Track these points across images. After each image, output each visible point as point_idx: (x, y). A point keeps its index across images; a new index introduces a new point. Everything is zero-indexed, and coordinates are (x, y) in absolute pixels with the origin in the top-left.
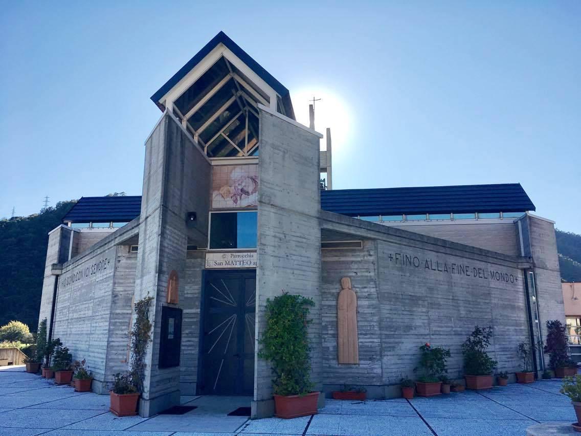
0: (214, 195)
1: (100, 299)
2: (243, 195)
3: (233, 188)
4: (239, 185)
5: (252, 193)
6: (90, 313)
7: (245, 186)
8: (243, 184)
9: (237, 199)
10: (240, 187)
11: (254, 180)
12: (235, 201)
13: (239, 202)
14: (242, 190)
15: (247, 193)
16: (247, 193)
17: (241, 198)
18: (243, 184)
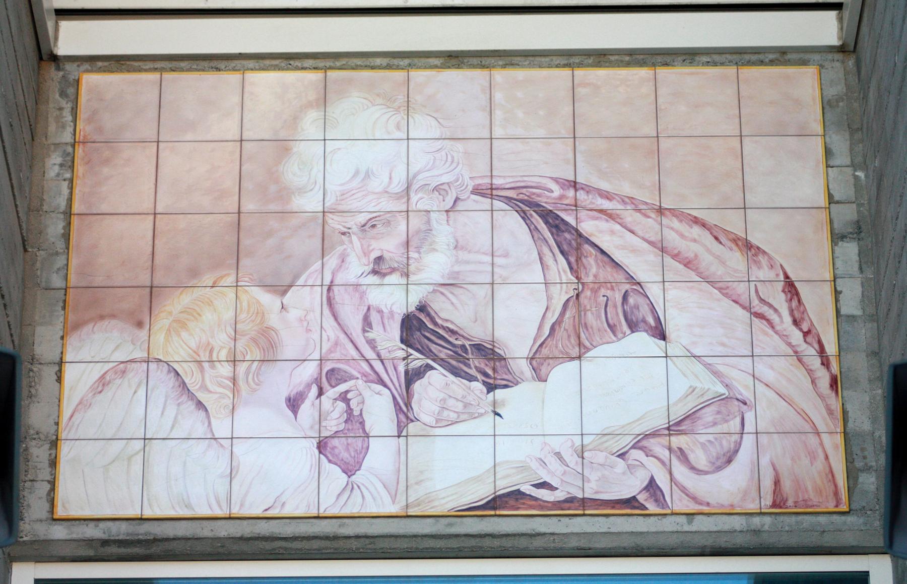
0: (78, 378)
2: (436, 386)
3: (305, 299)
4: (379, 267)
5: (540, 362)
7: (450, 285)
8: (434, 265)
9: (354, 420)
10: (394, 298)
11: (555, 226)
12: (341, 446)
13: (380, 456)
14: (416, 327)
15: (483, 363)
16: (483, 363)
17: (404, 412)
18: (434, 265)
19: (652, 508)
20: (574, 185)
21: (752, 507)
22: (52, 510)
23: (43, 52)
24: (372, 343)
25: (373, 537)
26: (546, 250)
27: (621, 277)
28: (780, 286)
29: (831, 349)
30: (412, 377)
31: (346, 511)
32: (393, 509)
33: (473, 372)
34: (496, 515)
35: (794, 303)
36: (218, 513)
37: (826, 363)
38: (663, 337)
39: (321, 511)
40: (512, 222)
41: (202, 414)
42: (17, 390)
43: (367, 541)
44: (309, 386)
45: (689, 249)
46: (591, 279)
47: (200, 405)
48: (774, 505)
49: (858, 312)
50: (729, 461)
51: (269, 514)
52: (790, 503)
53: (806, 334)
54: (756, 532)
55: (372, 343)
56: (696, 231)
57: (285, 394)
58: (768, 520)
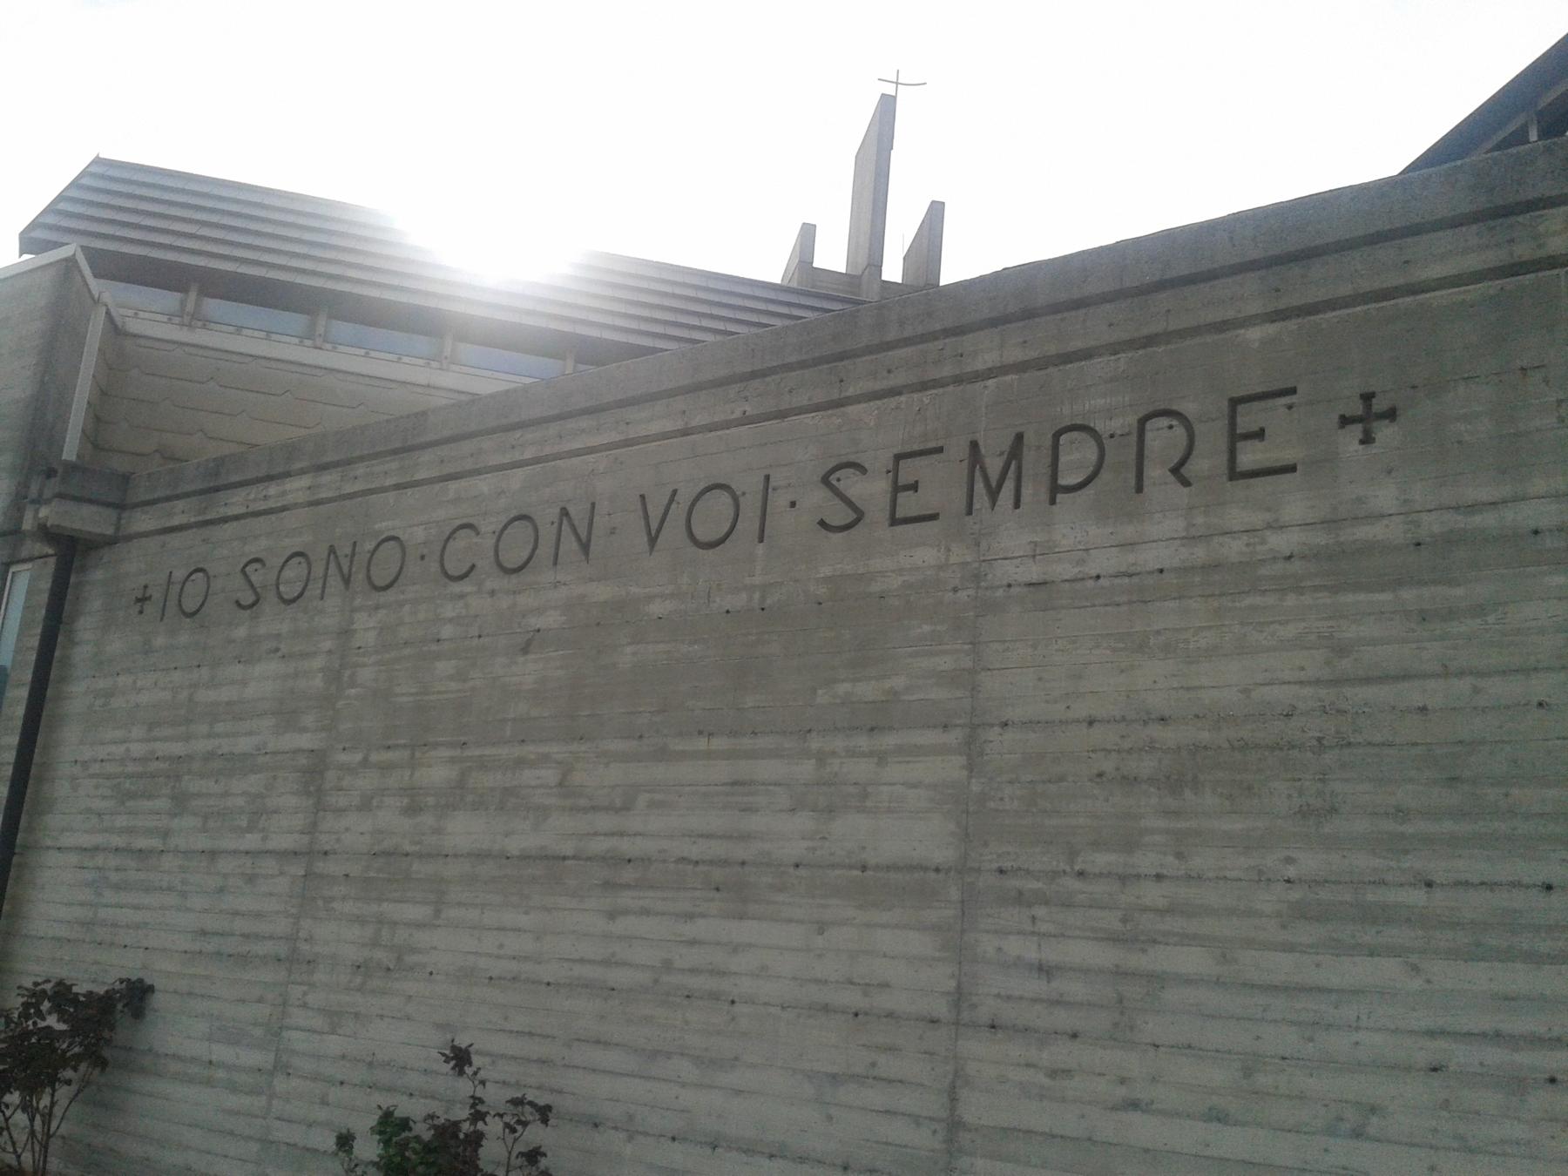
1: (1168, 736)
6: (926, 838)
12: (128, 750)
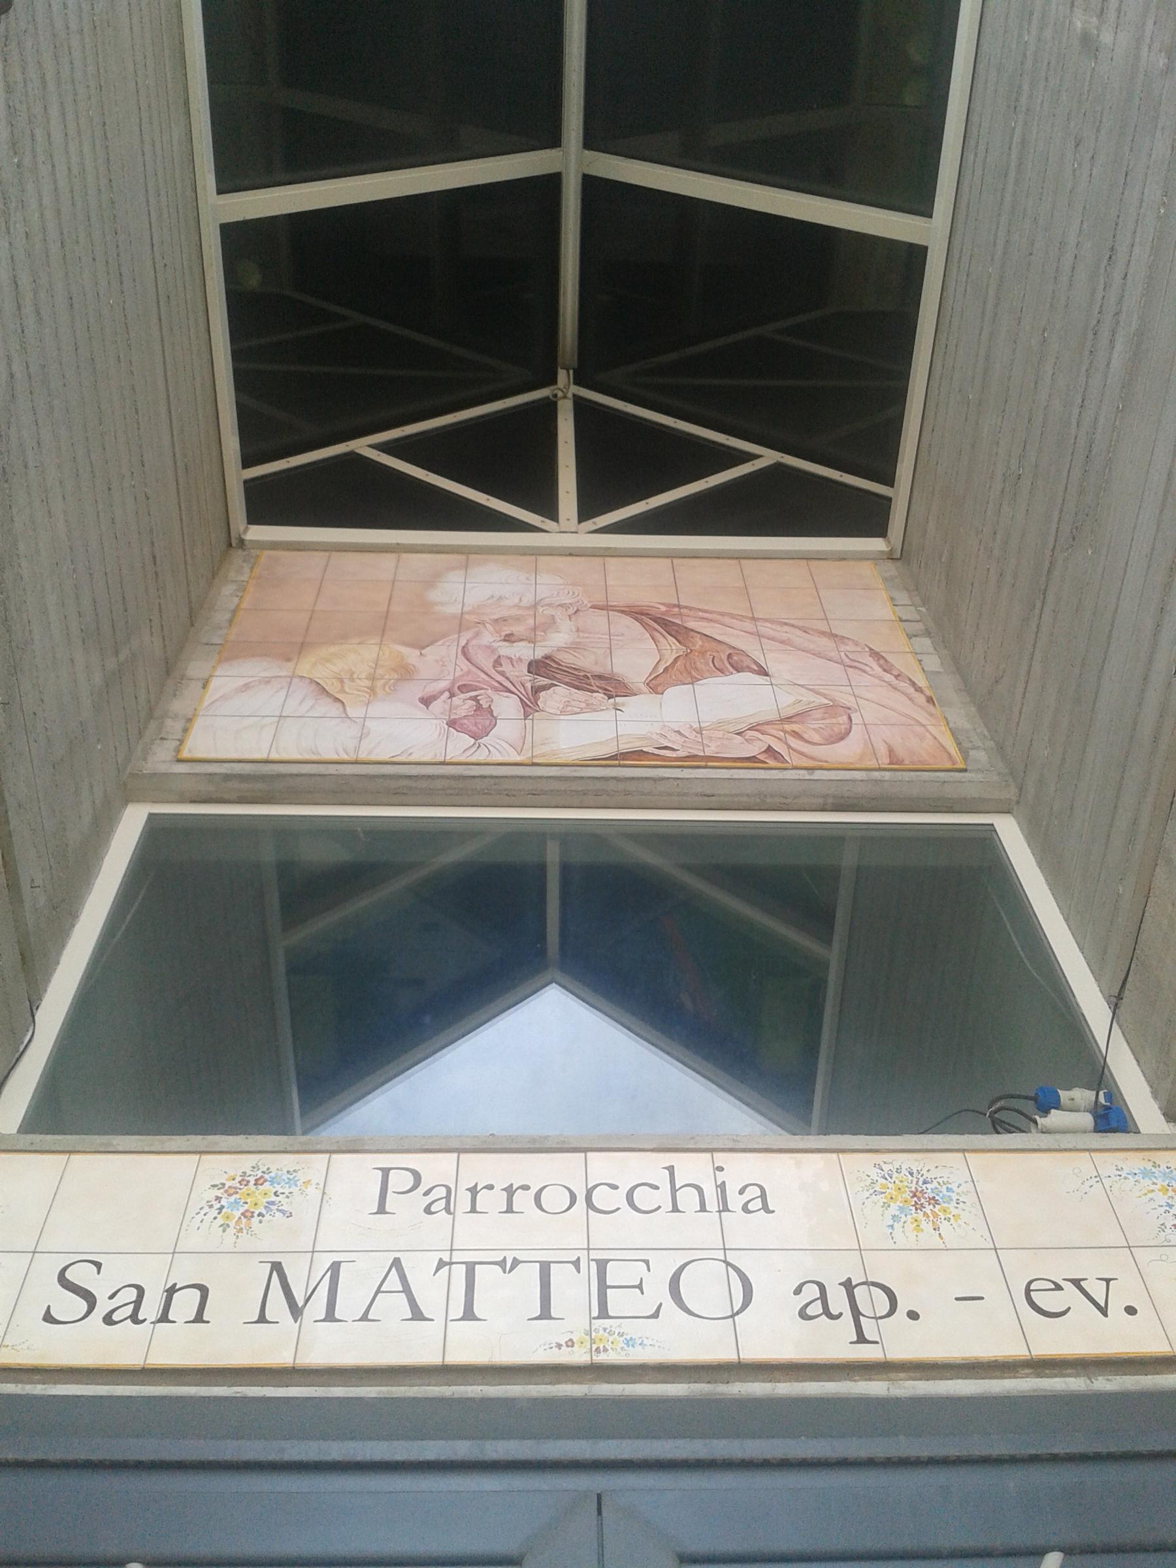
19: (772, 763)
20: (679, 606)
21: (872, 764)
22: (178, 750)
23: (233, 534)
24: (502, 674)
25: (497, 777)
26: (657, 635)
27: (723, 647)
28: (867, 654)
29: (922, 682)
30: (537, 690)
31: (474, 759)
32: (518, 759)
33: (595, 688)
34: (620, 766)
35: (882, 662)
36: (345, 757)
37: (919, 690)
38: (766, 674)
39: (448, 758)
40: (628, 621)
41: (339, 705)
42: (579, 211)
43: (492, 781)
44: (442, 693)
45: (785, 636)
46: (697, 647)
47: (337, 700)
48: (891, 763)
49: (941, 670)
50: (842, 739)
51: (394, 759)
52: (906, 762)
53: (896, 677)
54: (876, 781)
55: (502, 674)
56: (786, 628)
57: (420, 695)
58: (887, 775)
